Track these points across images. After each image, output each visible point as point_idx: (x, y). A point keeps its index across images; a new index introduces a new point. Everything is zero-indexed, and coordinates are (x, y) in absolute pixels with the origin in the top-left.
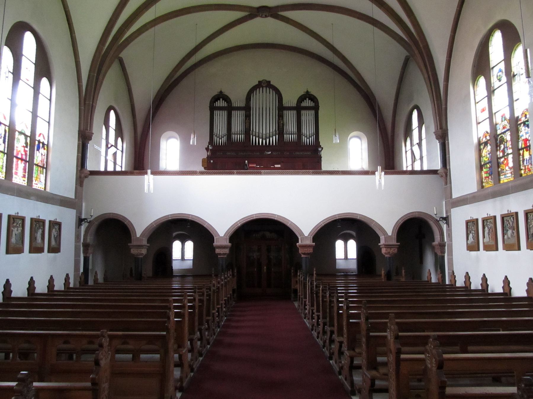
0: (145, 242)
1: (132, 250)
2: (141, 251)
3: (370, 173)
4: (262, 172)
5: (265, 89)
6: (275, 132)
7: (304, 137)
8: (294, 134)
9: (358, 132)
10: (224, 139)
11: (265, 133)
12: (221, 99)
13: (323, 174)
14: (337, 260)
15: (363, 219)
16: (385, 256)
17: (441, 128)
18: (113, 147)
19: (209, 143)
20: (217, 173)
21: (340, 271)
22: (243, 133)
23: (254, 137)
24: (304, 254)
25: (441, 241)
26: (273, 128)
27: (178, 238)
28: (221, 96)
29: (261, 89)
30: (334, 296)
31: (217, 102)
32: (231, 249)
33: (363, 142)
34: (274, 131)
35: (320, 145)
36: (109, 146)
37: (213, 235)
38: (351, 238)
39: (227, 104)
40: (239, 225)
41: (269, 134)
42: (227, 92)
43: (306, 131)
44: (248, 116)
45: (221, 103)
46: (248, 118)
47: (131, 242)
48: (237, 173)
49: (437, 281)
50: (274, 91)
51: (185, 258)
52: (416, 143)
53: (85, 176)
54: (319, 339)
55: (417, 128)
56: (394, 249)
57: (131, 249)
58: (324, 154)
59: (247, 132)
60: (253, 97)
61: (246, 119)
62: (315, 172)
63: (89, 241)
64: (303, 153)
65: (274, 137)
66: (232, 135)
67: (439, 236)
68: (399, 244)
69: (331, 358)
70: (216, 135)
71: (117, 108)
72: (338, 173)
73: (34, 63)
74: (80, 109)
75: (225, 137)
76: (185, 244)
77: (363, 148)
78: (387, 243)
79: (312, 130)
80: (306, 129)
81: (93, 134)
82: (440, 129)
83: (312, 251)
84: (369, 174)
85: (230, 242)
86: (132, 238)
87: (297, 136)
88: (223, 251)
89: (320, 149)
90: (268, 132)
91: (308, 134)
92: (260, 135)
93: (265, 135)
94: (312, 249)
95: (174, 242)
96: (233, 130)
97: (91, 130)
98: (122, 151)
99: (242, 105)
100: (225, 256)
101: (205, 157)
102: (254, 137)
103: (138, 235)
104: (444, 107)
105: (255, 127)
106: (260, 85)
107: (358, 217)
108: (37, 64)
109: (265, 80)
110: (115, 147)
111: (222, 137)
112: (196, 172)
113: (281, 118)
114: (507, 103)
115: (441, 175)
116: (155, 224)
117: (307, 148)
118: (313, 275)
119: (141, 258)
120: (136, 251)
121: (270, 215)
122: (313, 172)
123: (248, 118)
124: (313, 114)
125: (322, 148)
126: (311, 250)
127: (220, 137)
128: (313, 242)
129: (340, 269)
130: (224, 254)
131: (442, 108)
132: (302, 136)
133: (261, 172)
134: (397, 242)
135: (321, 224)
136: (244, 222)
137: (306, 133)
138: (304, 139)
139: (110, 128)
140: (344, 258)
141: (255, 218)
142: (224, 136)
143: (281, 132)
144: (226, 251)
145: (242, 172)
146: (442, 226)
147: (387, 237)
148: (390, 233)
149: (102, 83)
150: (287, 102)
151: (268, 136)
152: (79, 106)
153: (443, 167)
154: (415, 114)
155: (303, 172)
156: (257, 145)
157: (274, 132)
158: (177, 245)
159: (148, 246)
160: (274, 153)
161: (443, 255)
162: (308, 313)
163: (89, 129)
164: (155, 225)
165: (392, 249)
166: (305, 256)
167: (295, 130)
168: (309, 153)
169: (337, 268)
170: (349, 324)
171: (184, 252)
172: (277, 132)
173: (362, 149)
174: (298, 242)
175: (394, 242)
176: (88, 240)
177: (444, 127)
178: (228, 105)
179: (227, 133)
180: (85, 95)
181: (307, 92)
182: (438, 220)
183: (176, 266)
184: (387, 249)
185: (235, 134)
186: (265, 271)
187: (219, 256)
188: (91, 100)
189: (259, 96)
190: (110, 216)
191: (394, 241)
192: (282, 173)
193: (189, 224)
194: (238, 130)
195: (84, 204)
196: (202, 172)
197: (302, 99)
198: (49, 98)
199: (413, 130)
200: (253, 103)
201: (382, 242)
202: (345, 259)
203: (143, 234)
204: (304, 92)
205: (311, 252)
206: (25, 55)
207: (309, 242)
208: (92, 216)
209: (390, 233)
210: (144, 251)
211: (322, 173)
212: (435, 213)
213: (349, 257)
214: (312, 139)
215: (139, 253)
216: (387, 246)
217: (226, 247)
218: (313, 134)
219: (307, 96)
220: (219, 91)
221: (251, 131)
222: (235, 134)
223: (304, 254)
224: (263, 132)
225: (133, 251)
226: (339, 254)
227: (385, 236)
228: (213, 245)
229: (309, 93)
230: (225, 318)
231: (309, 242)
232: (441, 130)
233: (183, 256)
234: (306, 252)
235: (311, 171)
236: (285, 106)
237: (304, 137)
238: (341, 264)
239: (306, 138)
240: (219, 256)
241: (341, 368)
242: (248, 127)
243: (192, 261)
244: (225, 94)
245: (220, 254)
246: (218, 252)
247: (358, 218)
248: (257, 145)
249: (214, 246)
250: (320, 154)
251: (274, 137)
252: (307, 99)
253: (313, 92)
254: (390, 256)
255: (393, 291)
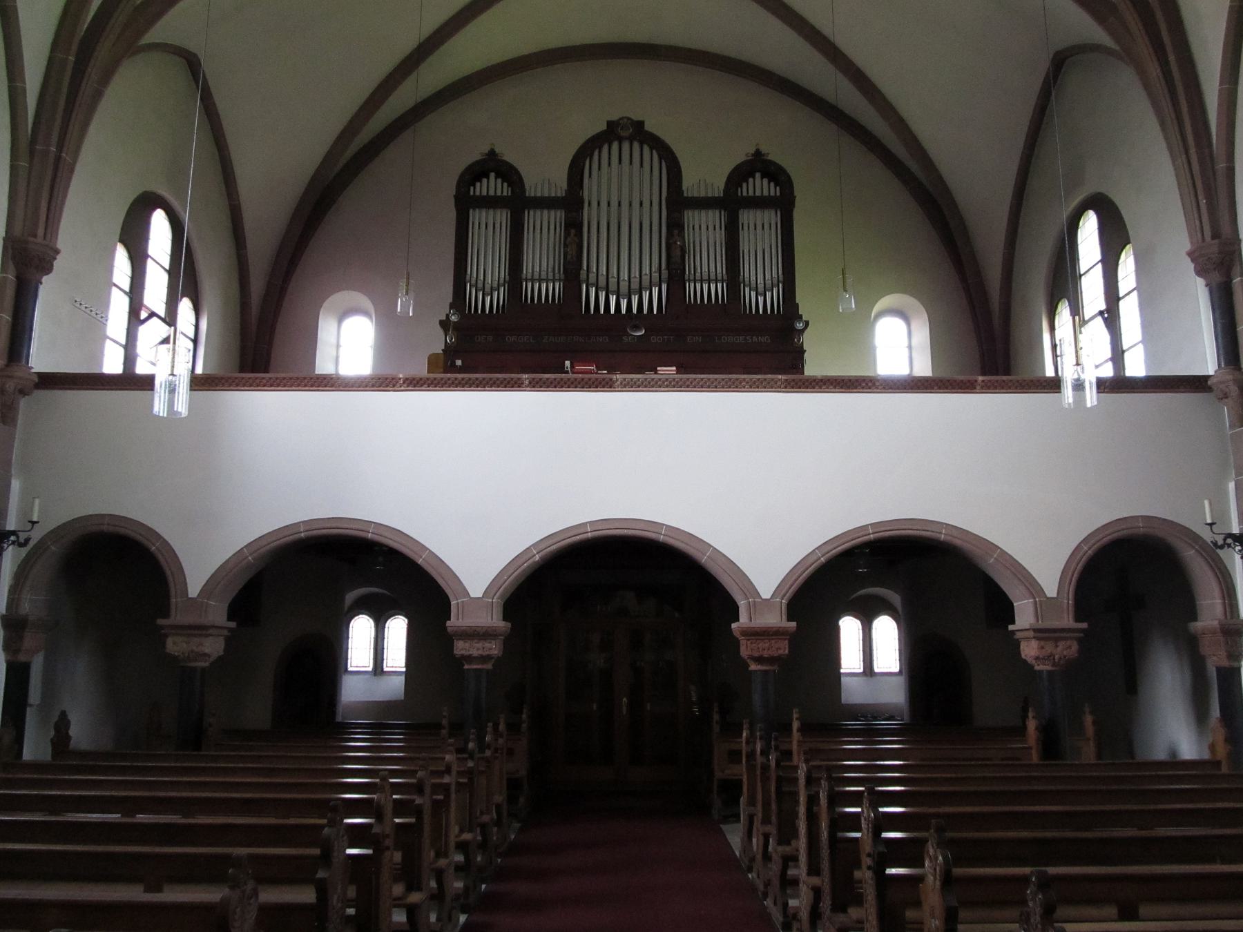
0: (218, 614)
1: (169, 641)
2: (201, 644)
3: (978, 387)
4: (617, 380)
5: (626, 146)
6: (657, 274)
7: (747, 290)
8: (716, 281)
9: (905, 296)
10: (500, 296)
11: (626, 279)
12: (492, 175)
13: (821, 388)
14: (843, 679)
15: (958, 542)
16: (1033, 667)
17: (1216, 235)
18: (155, 319)
19: (452, 306)
20: (464, 382)
21: (857, 712)
22: (557, 277)
23: (593, 291)
24: (759, 660)
25: (1226, 617)
26: (651, 261)
27: (362, 606)
28: (490, 165)
29: (615, 146)
30: (819, 779)
31: (478, 184)
32: (509, 641)
33: (915, 325)
34: (653, 270)
35: (800, 313)
36: (144, 315)
37: (448, 591)
38: (880, 612)
39: (510, 189)
40: (537, 558)
41: (638, 280)
42: (509, 155)
43: (753, 272)
44: (574, 226)
45: (492, 186)
46: (573, 231)
47: (166, 614)
48: (530, 383)
49: (1206, 755)
50: (654, 151)
51: (386, 669)
52: (1097, 311)
53: (20, 387)
54: (768, 900)
55: (1100, 266)
56: (1069, 643)
57: (166, 636)
58: (809, 341)
59: (572, 273)
60: (590, 176)
61: (567, 234)
62: (794, 380)
63: (27, 610)
64: (745, 339)
65: (655, 291)
66: (524, 283)
67: (1219, 601)
68: (1084, 625)
69: (750, 870)
70: (473, 282)
71: (175, 203)
72: (870, 384)
73: (167, 268)
74: (13, 169)
75: (502, 289)
76: (387, 625)
77: (915, 342)
78: (1041, 625)
79: (775, 271)
80: (753, 268)
81: (57, 252)
82: (1213, 238)
83: (787, 651)
84: (975, 388)
85: (506, 617)
86: (173, 600)
87: (727, 286)
88: (478, 649)
89: (800, 326)
90: (635, 272)
91: (760, 280)
92: (613, 281)
93: (627, 283)
94: (787, 641)
95: (353, 621)
96: (527, 270)
97: (49, 236)
98: (195, 341)
99: (556, 192)
100: (489, 666)
101: (439, 348)
102: (593, 291)
103: (194, 590)
104: (1221, 165)
105: (596, 262)
106: (612, 133)
107: (941, 533)
108: (172, 272)
109: (629, 119)
110: (163, 320)
111: (492, 289)
112: (393, 379)
113: (676, 232)
114: (1108, 353)
115: (1222, 391)
116: (251, 555)
117: (760, 322)
118: (787, 728)
119: (203, 669)
120: (185, 645)
121: (642, 526)
122: (786, 380)
123: (573, 231)
124: (777, 224)
125: (807, 323)
126: (782, 648)
127: (488, 289)
128: (789, 619)
129: (856, 705)
130: (484, 659)
131: (1214, 173)
132: (742, 285)
133: (611, 380)
134: (1078, 619)
135: (815, 558)
136: (554, 547)
137: (753, 278)
138: (749, 295)
139: (150, 265)
140: (861, 670)
141: (590, 535)
142: (499, 286)
143: (676, 276)
144: (490, 649)
145: (548, 379)
146: (1228, 567)
147: (1042, 604)
148: (1051, 590)
149: (98, 95)
150: (696, 187)
151: (635, 286)
152: (11, 157)
153: (1226, 364)
154: (1089, 230)
155: (755, 382)
156: (602, 312)
157: (656, 275)
158: (361, 629)
159: (230, 630)
160: (655, 339)
161: (1235, 664)
162: (804, 915)
163: (41, 232)
164: (250, 558)
165: (1061, 644)
166: (759, 667)
167: (721, 269)
168: (764, 339)
169: (844, 700)
170: (883, 881)
171: (383, 648)
172: (665, 273)
173: (910, 347)
174: (738, 620)
175: (1067, 621)
176: (26, 608)
177: (1226, 230)
178: (512, 191)
179: (507, 278)
180: (34, 123)
181: (758, 153)
182: (1220, 542)
183: (352, 692)
184: (1042, 643)
185: (533, 280)
186: (625, 713)
187: (466, 667)
188: (55, 138)
189: (610, 173)
190: (103, 524)
191: (1066, 616)
192: (685, 382)
193: (381, 559)
194: (646, 270)
195: (16, 485)
196: (414, 379)
197: (740, 175)
198: (192, 336)
199: (1081, 276)
200: (591, 188)
201: (1024, 616)
202: (864, 673)
203: (208, 589)
204: (747, 155)
205: (781, 652)
206: (152, 256)
207: (775, 619)
208: (33, 523)
209: (1051, 590)
210: (213, 647)
211: (817, 384)
212: (1209, 521)
213: (878, 668)
214: (774, 296)
215: (192, 651)
216: (1042, 634)
217: (490, 635)
218: (775, 281)
219: (758, 165)
220: (487, 152)
221: (581, 272)
222: (533, 280)
223: (759, 660)
224: (621, 274)
225: (175, 646)
226: (359, 653)
227: (1035, 598)
228: (445, 628)
229: (765, 158)
230: (463, 918)
231: (775, 619)
232: (1216, 241)
233: (379, 662)
234: (766, 654)
235: (780, 377)
236: (690, 195)
237: (747, 290)
238: (854, 692)
239: (753, 294)
240: (466, 667)
241: (767, 884)
242: (575, 258)
243: (403, 678)
244: (506, 158)
245: (470, 659)
246: (463, 652)
247: (943, 536)
248: (602, 312)
249: (449, 629)
250: (799, 341)
251: (655, 291)
252: (758, 175)
253: (775, 155)
254: (1054, 669)
255: (1053, 788)
